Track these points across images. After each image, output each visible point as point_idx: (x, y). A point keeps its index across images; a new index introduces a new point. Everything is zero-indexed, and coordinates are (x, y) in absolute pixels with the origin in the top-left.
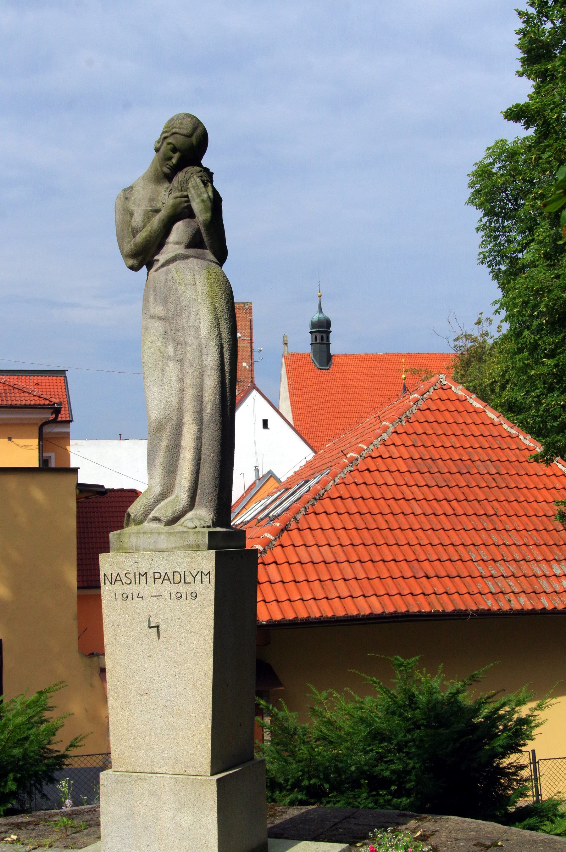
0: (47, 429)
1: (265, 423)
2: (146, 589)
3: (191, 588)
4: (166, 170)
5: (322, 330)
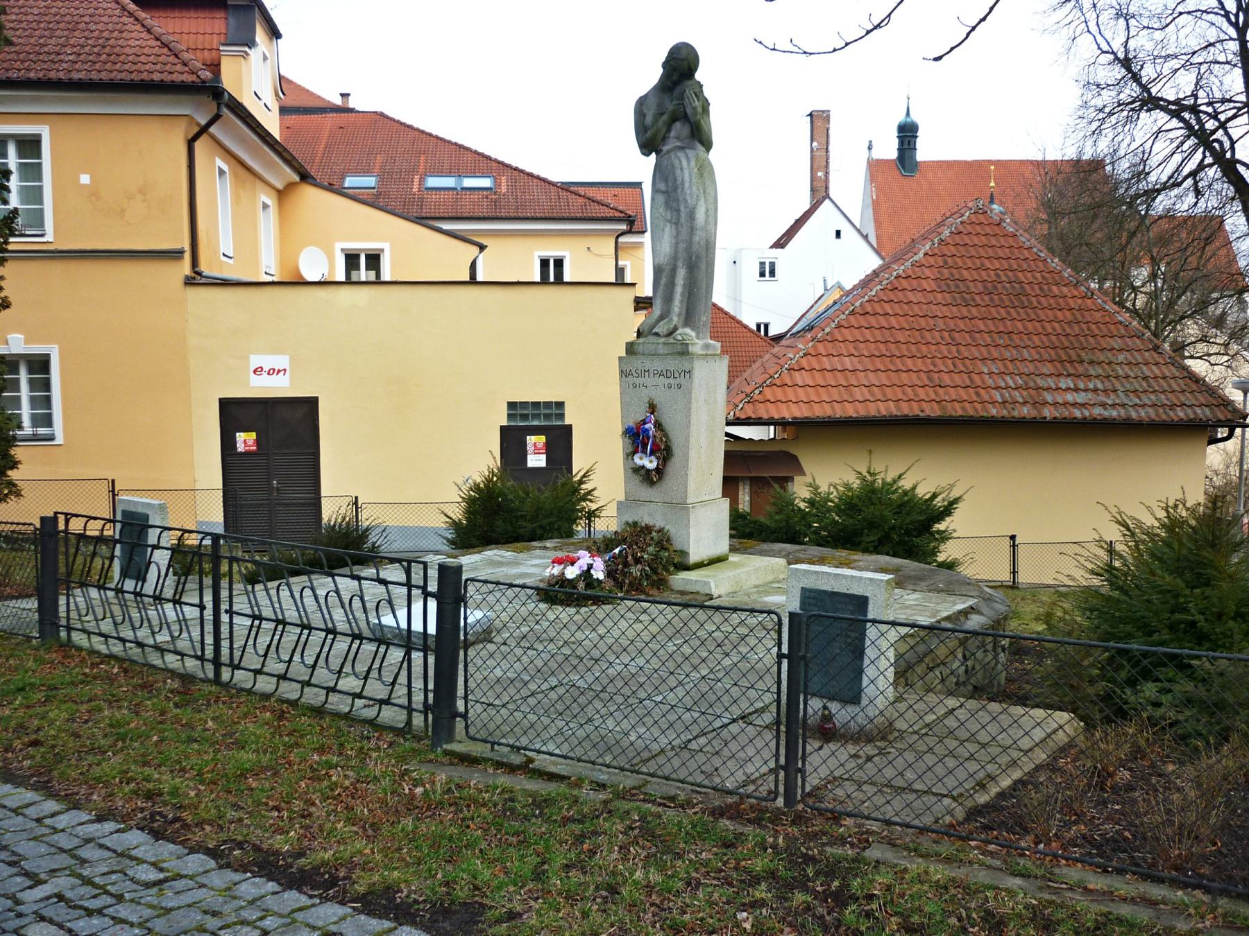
0: (621, 240)
1: (838, 234)
2: (649, 381)
3: (677, 381)
4: (669, 84)
5: (907, 133)
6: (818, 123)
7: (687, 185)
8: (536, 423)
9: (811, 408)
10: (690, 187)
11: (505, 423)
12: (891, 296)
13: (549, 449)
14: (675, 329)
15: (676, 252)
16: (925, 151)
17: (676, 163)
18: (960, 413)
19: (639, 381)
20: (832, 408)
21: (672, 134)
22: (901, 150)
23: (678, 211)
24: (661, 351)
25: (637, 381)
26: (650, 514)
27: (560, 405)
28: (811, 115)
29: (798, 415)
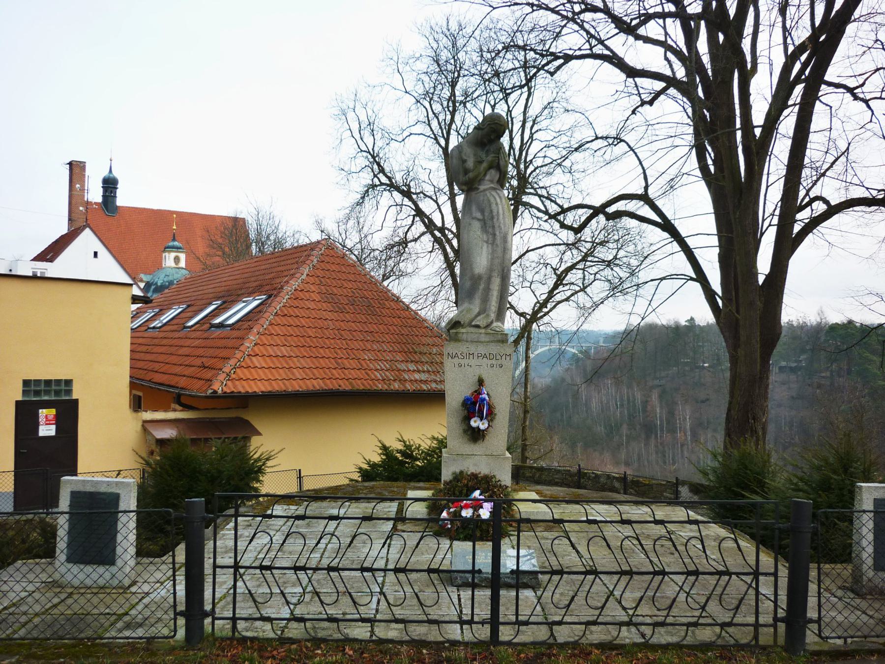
1: (96, 254)
2: (473, 362)
3: (499, 362)
6: (76, 170)
7: (501, 216)
8: (46, 398)
9: (271, 384)
10: (504, 218)
11: (20, 398)
12: (296, 303)
13: (59, 421)
14: (492, 322)
15: (492, 264)
16: (123, 199)
17: (492, 200)
18: (362, 387)
19: (466, 361)
20: (284, 384)
21: (488, 177)
22: (104, 196)
23: (494, 235)
24: (483, 340)
25: (462, 362)
26: (475, 465)
27: (69, 382)
28: (70, 164)
29: (263, 389)
